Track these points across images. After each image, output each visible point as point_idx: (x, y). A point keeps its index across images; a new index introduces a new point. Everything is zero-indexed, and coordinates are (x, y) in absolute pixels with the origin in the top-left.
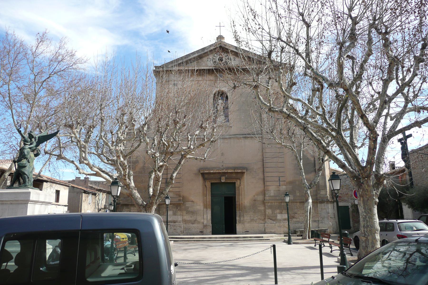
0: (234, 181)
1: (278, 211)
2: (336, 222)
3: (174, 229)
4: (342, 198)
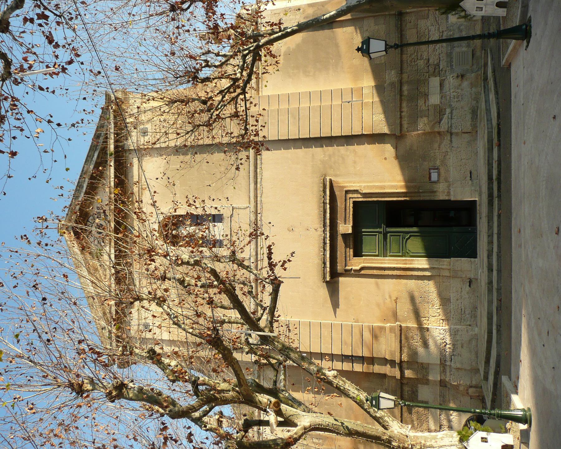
0: (352, 205)
1: (421, 102)
3: (462, 347)
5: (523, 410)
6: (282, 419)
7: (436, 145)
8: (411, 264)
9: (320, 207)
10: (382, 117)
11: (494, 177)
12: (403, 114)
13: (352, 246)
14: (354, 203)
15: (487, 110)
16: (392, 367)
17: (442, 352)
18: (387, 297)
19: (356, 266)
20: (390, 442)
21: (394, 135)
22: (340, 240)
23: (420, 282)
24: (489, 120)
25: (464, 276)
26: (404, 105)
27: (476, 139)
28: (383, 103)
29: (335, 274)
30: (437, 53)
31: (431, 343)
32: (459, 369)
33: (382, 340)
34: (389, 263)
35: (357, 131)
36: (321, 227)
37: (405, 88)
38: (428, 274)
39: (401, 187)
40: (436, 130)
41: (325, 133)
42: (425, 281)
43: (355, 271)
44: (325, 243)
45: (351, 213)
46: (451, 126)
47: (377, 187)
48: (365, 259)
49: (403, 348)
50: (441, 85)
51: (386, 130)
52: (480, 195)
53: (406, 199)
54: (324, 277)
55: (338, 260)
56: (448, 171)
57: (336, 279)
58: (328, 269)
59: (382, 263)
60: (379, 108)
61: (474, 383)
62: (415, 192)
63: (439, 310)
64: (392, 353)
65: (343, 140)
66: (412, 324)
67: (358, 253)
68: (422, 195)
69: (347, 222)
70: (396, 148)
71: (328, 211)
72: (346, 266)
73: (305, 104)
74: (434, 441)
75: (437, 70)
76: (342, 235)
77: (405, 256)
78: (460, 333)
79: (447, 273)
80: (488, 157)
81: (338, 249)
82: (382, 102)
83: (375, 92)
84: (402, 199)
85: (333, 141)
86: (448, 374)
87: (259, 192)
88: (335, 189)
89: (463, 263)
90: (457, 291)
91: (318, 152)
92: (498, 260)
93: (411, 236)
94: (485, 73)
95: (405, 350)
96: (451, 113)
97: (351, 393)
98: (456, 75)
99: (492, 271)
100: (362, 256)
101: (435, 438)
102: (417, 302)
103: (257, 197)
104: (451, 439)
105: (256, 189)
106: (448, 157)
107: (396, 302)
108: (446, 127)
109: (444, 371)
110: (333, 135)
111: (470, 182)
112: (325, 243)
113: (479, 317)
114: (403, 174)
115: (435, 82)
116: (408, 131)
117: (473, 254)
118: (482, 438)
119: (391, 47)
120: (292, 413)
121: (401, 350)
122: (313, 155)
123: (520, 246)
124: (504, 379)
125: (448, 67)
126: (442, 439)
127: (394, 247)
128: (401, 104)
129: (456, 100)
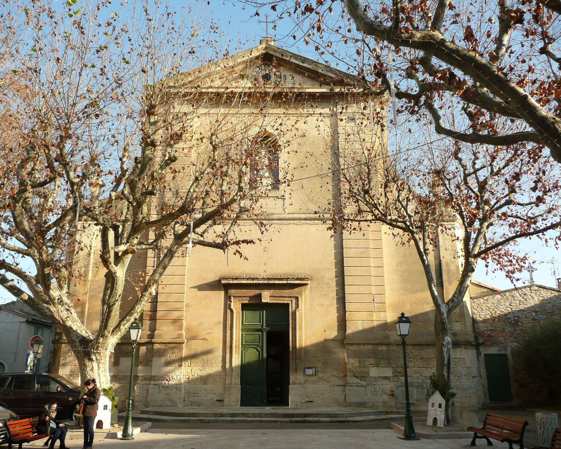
0: (286, 302)
1: (372, 361)
2: (483, 384)
3: (166, 394)
4: (493, 339)
5: (132, 435)
6: (120, 254)
7: (335, 373)
8: (236, 352)
9: (285, 275)
10: (360, 328)
11: (306, 419)
12: (362, 346)
13: (251, 302)
14: (288, 304)
15: (361, 413)
16: (148, 335)
17: (162, 378)
18: (208, 332)
19: (234, 305)
20: (103, 336)
21: (345, 339)
22: (257, 292)
23: (221, 359)
24: (352, 415)
25: (226, 395)
26: (370, 347)
27: (339, 405)
28: (372, 330)
29: (227, 287)
30: (413, 375)
31: (170, 368)
32: (148, 391)
33: (171, 328)
34: (236, 333)
35: (348, 307)
36: (267, 276)
37: (384, 348)
38: (228, 366)
39: (301, 344)
40: (348, 374)
41: (347, 280)
42: (221, 364)
43: (230, 305)
44: (253, 279)
45: (279, 302)
46: (351, 386)
47: (301, 321)
48: (239, 313)
49: (164, 345)
50: (386, 378)
51: (349, 331)
52: (293, 409)
53: (291, 348)
54: (224, 279)
55: (239, 290)
56: (314, 383)
57: (223, 288)
58: (231, 282)
59: (236, 327)
60: (367, 325)
61: (136, 404)
62: (296, 355)
63: (196, 375)
64: (160, 336)
65: (341, 295)
66: (184, 353)
67: (245, 307)
68: (294, 361)
69: (272, 298)
70: (333, 340)
71: (281, 282)
72: (234, 297)
73: (372, 262)
74: (103, 369)
75: (398, 374)
76: (261, 294)
77: (242, 347)
78: (178, 392)
79: (228, 382)
80: (323, 414)
81: (248, 290)
82: (373, 328)
83: (382, 322)
84: (291, 345)
85: (341, 287)
86: (144, 382)
87: (298, 221)
88: (299, 288)
89: (236, 395)
90: (213, 390)
91: (331, 274)
92: (241, 420)
93: (259, 352)
94: (392, 413)
95: (163, 347)
96: (362, 386)
97: (138, 306)
98: (393, 390)
99: (232, 417)
100: (242, 310)
101: (105, 370)
102: (204, 357)
103: (293, 220)
104: (105, 382)
105: (300, 219)
106: (326, 383)
107: (203, 339)
108: (350, 382)
109: (145, 378)
110: (346, 287)
111: (304, 401)
112: (253, 279)
113: (192, 407)
114: (312, 346)
115: (388, 372)
116: (347, 350)
117: (244, 403)
118: (107, 406)
119: (403, 339)
120: (125, 262)
121: (163, 343)
122: (329, 269)
123: (253, 434)
124: (149, 424)
125: (401, 383)
126: (105, 376)
127: (250, 338)
128: (370, 344)
129: (373, 390)
